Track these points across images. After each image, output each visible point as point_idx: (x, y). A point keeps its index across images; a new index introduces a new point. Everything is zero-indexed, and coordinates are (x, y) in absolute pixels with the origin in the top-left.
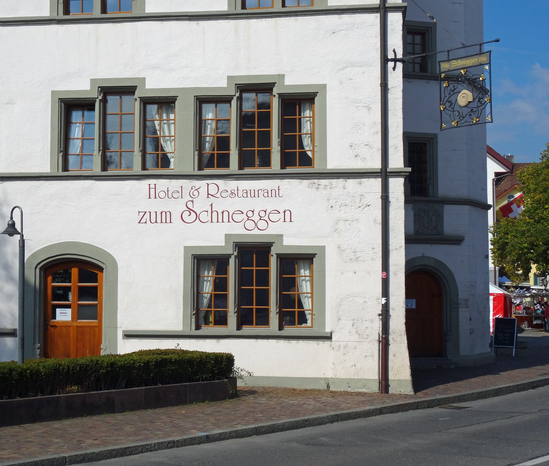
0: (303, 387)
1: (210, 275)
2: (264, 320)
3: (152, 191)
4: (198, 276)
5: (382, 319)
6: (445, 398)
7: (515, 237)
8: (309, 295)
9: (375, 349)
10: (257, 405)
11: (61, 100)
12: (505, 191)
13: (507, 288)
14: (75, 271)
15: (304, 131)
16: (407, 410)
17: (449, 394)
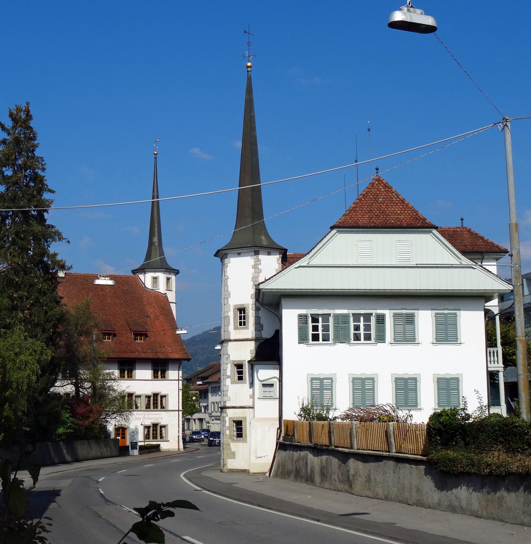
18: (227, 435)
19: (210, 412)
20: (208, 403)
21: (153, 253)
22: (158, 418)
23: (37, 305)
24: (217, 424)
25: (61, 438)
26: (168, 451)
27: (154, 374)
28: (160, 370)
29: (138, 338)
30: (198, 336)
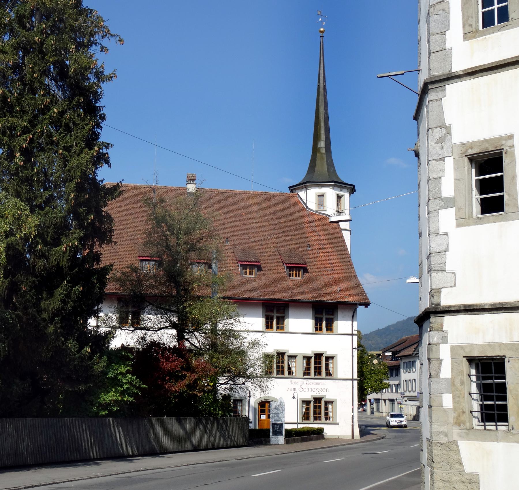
3: (291, 382)
9: (350, 427)
18: (445, 411)
19: (403, 391)
20: (400, 380)
21: (318, 162)
23: (50, 149)
24: (411, 405)
25: (110, 411)
26: (337, 440)
27: (316, 324)
28: (324, 319)
29: (293, 274)
30: (393, 325)
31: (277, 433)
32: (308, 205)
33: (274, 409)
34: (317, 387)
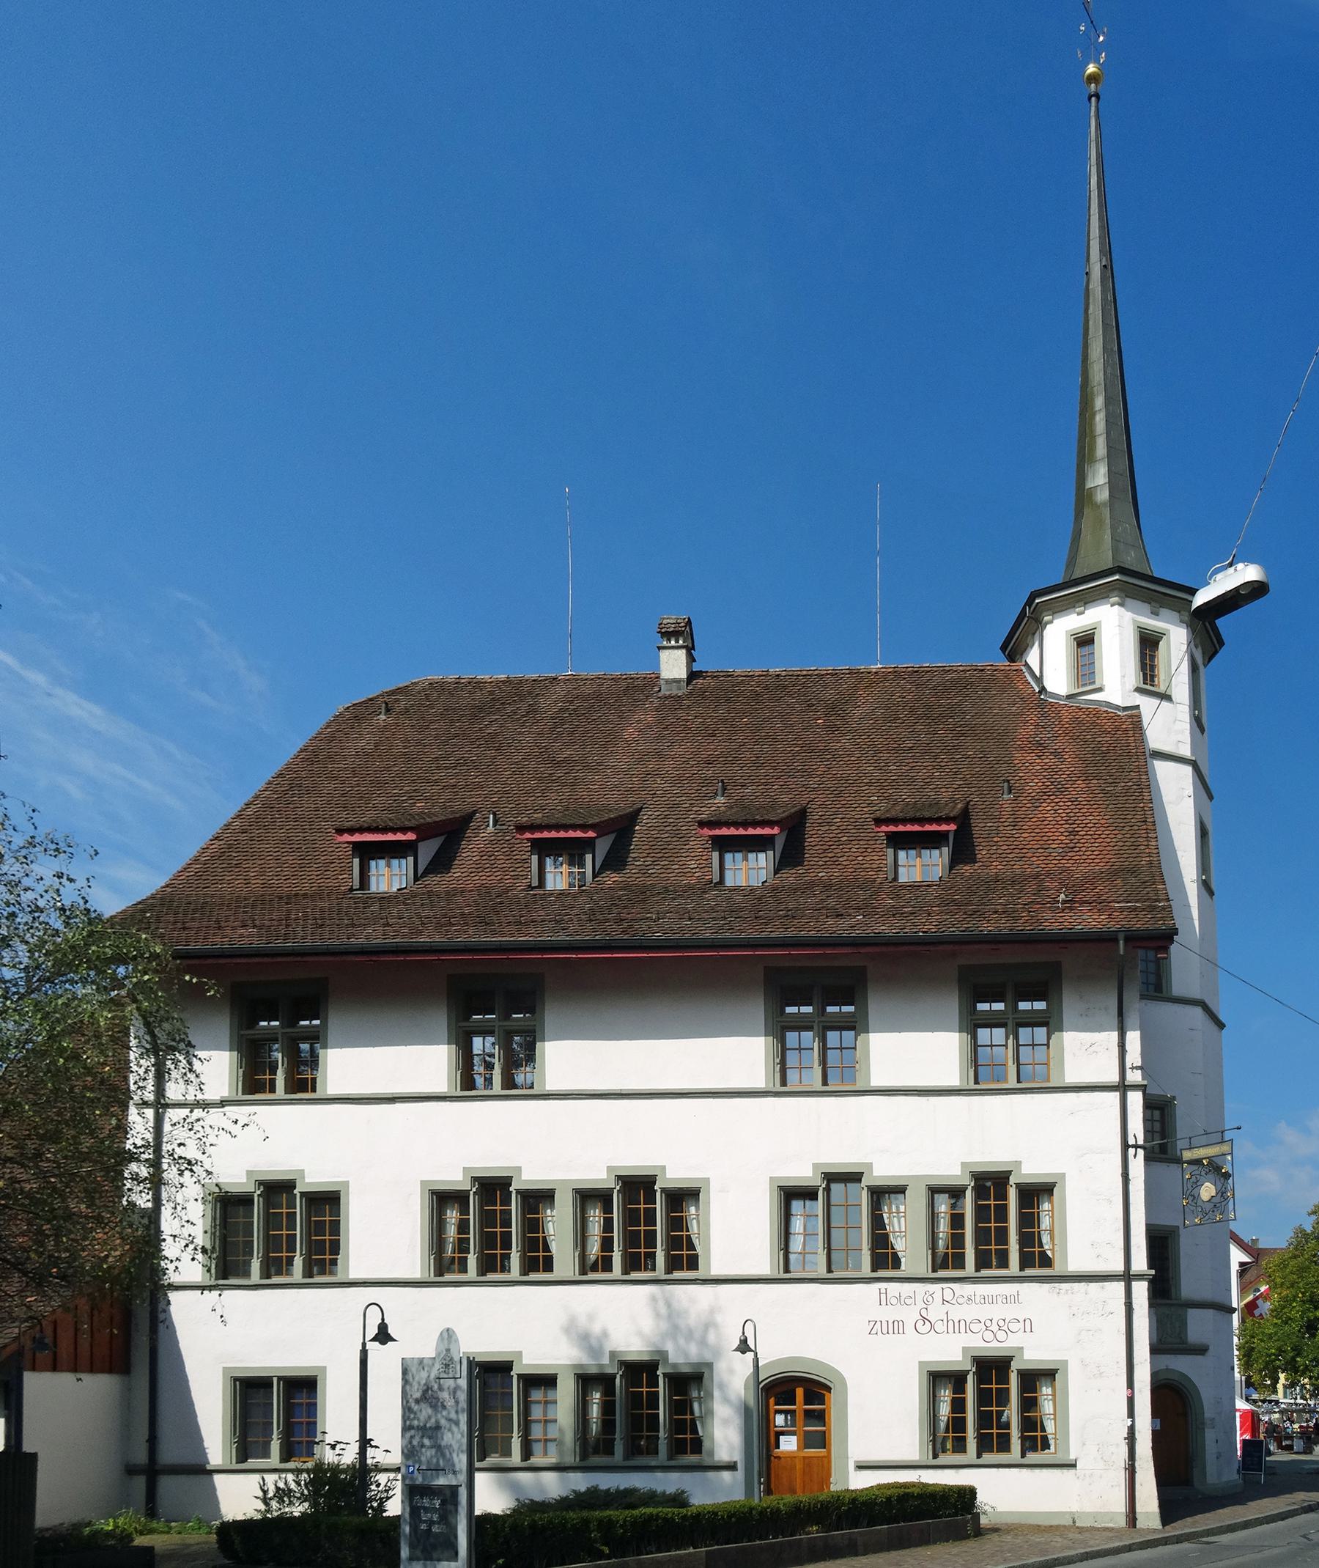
0: (1047, 1523)
1: (947, 1394)
2: (1004, 1446)
3: (883, 1296)
4: (934, 1396)
5: (1128, 1444)
6: (1193, 1532)
7: (1262, 1340)
8: (1052, 1417)
9: (1121, 1477)
10: (1003, 1544)
11: (781, 1188)
12: (1251, 1283)
13: (1255, 1401)
14: (800, 1392)
15: (1043, 1226)
16: (1156, 1546)
17: (1198, 1527)
22: (1004, 1325)
31: (434, 1547)
32: (1046, 684)
33: (417, 1401)
34: (984, 1312)
